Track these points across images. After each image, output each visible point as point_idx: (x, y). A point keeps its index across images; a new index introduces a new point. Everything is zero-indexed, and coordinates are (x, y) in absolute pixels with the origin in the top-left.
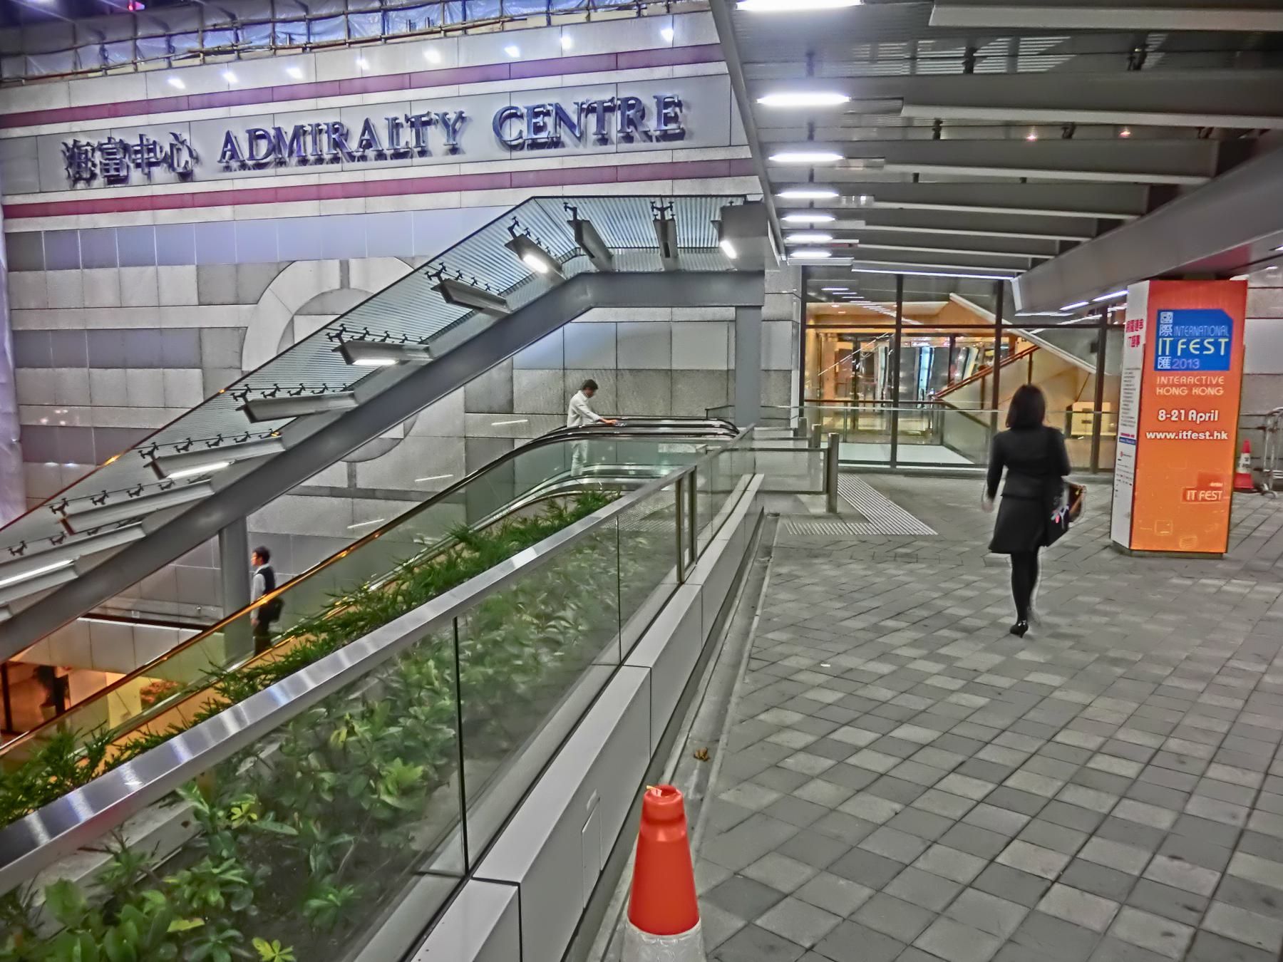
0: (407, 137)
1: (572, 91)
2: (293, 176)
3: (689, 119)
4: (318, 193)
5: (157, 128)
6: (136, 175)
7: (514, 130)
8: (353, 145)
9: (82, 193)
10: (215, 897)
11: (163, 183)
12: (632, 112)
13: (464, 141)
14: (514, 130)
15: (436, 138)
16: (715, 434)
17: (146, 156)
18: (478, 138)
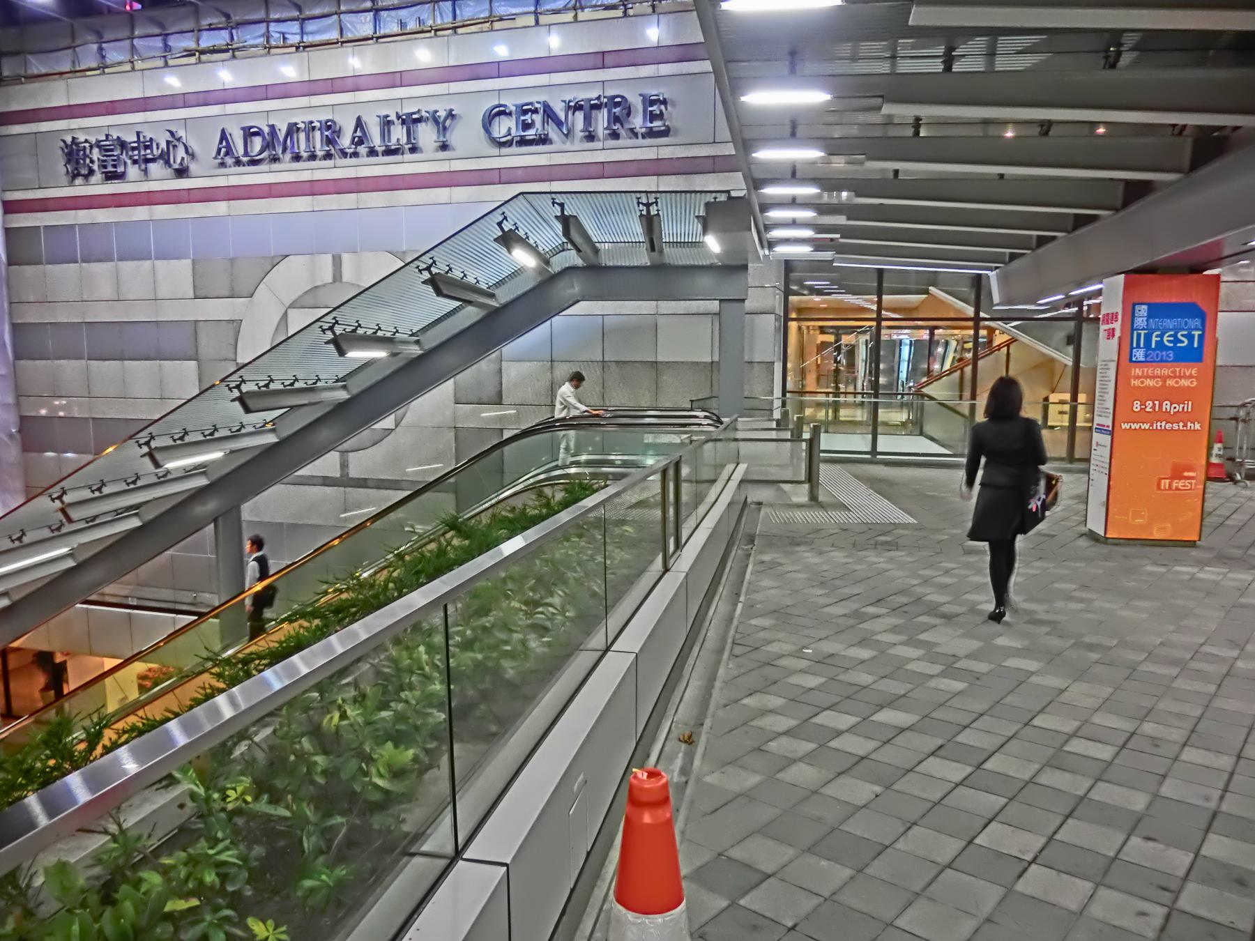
0: (398, 134)
1: (560, 89)
2: (287, 172)
3: (674, 117)
4: (311, 189)
5: (154, 125)
6: (133, 171)
7: (503, 127)
8: (345, 142)
9: (80, 189)
10: (210, 878)
11: (160, 179)
12: (618, 109)
13: (453, 138)
14: (503, 127)
15: (427, 135)
16: (699, 425)
17: (142, 152)
18: (467, 135)
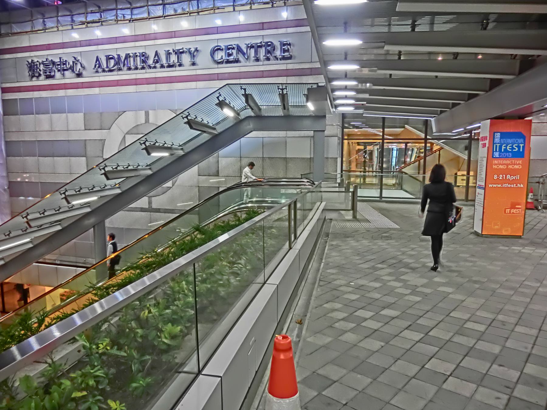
0: (174, 58)
1: (244, 39)
2: (125, 75)
3: (294, 51)
4: (136, 82)
5: (67, 54)
6: (58, 75)
7: (219, 55)
8: (150, 62)
9: (35, 82)
10: (91, 382)
11: (70, 78)
12: (270, 48)
13: (198, 60)
14: (219, 55)
15: (186, 59)
16: (305, 185)
17: (62, 66)
18: (204, 59)
